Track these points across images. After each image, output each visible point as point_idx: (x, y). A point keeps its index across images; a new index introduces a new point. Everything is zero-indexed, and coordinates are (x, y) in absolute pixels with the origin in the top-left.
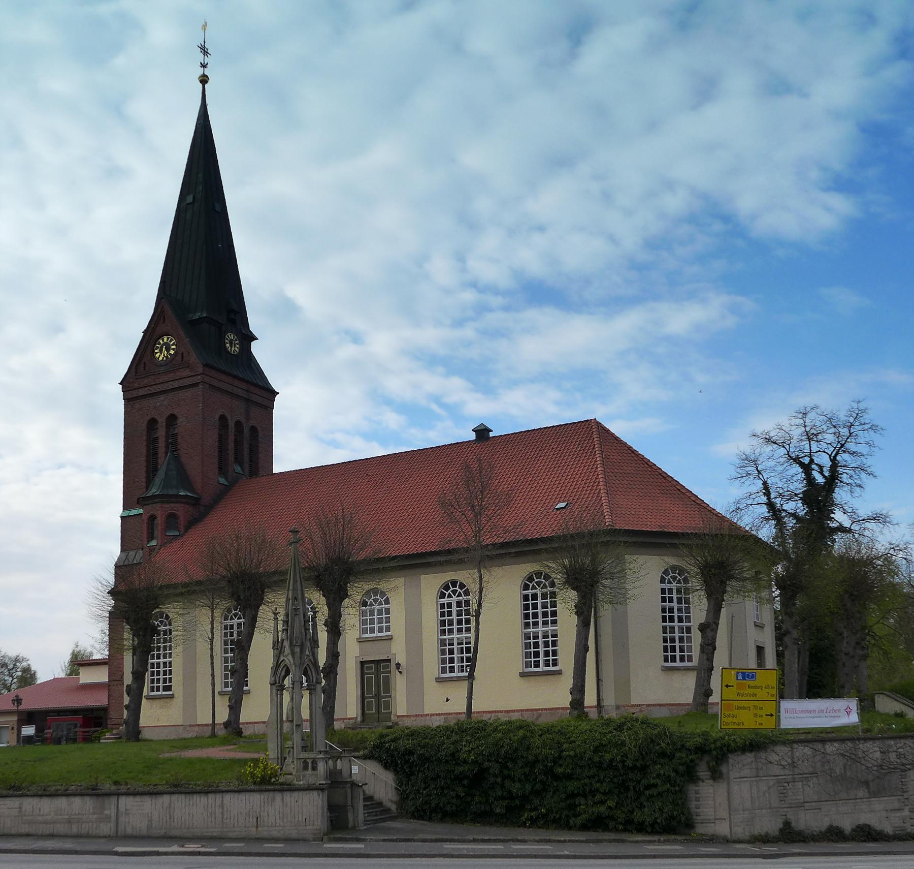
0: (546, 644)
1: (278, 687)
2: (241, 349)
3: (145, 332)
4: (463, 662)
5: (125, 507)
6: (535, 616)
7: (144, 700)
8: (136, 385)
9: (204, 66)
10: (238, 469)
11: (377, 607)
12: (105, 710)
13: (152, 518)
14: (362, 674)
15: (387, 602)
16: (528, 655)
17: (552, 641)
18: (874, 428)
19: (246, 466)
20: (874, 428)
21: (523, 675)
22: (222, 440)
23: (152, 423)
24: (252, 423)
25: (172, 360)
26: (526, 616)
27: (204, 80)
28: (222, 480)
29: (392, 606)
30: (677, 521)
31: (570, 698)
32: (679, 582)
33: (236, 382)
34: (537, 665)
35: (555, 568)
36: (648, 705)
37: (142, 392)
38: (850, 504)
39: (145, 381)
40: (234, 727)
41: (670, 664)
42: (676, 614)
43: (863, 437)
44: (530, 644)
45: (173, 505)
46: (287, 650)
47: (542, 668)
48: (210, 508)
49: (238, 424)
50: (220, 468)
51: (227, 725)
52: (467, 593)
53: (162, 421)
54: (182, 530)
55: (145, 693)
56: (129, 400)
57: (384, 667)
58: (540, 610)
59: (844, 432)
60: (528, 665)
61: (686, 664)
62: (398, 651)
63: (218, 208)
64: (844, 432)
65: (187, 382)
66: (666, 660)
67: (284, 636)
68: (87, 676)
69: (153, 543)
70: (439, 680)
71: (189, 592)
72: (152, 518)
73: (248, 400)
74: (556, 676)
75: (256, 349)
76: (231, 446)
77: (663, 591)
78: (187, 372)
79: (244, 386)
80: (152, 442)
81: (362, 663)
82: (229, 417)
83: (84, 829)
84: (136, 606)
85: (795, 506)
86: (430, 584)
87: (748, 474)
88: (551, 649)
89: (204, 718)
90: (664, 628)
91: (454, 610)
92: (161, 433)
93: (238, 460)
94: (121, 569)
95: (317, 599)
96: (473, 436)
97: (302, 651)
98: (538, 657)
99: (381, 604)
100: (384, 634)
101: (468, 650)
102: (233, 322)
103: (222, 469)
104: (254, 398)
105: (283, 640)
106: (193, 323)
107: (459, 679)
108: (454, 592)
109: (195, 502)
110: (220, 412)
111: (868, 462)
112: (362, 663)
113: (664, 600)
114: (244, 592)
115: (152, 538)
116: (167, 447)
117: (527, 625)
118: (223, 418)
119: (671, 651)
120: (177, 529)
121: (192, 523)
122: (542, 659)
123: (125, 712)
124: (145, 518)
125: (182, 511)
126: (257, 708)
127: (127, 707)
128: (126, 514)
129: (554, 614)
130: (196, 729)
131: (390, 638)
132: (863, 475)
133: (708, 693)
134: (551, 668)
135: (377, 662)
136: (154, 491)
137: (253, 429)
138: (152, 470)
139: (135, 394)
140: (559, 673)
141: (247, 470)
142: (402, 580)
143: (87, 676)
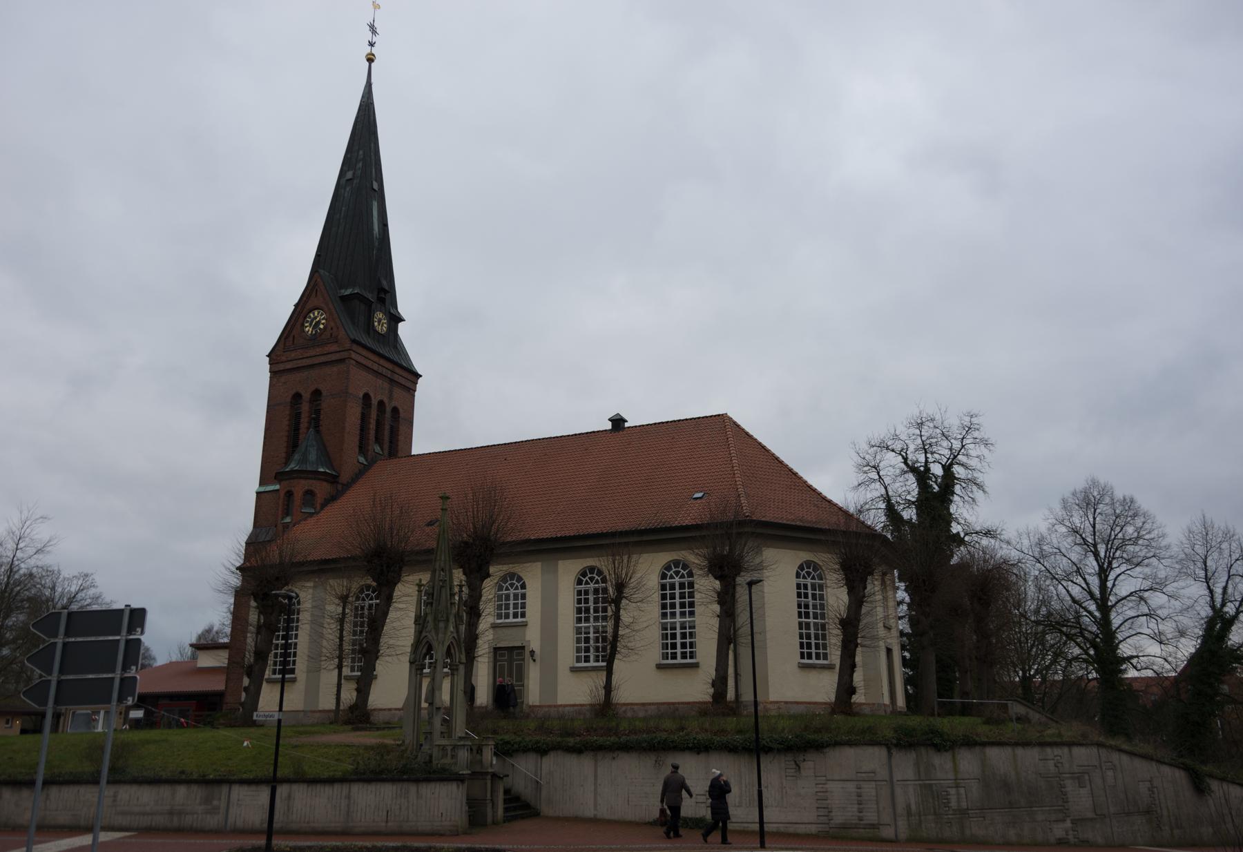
0: (684, 636)
1: (416, 665)
2: (389, 328)
3: (296, 306)
4: (604, 649)
5: (261, 483)
6: (673, 606)
7: (264, 684)
8: (284, 358)
9: (372, 44)
10: (378, 449)
11: (512, 591)
12: (220, 695)
13: (289, 494)
14: (495, 661)
15: (523, 587)
16: (665, 646)
17: (689, 633)
18: (986, 444)
19: (386, 446)
20: (986, 444)
21: (660, 667)
22: (364, 418)
23: (297, 397)
24: (394, 404)
25: (321, 334)
26: (664, 606)
27: (370, 59)
28: (362, 459)
29: (529, 592)
30: (808, 516)
31: (712, 691)
32: (813, 578)
33: (382, 362)
34: (674, 656)
35: (693, 558)
36: (786, 703)
37: (289, 366)
38: (968, 513)
39: (293, 355)
40: (359, 716)
41: (806, 661)
42: (811, 610)
43: (973, 450)
44: (668, 635)
45: (311, 481)
46: (430, 625)
47: (679, 660)
48: (347, 486)
49: (381, 403)
50: (360, 447)
51: (352, 708)
52: (604, 580)
53: (306, 396)
54: (318, 506)
55: (266, 677)
56: (274, 373)
57: (518, 654)
58: (677, 601)
59: (957, 445)
60: (665, 656)
61: (821, 662)
62: (533, 638)
63: (375, 186)
64: (957, 445)
65: (334, 357)
66: (802, 657)
67: (428, 610)
68: (207, 660)
69: (288, 520)
70: (574, 670)
71: (323, 568)
72: (289, 494)
73: (391, 381)
74: (688, 671)
75: (402, 329)
76: (373, 426)
77: (798, 586)
78: (334, 348)
79: (390, 366)
80: (296, 418)
81: (496, 649)
82: (372, 395)
83: (188, 821)
84: (265, 582)
85: (909, 514)
86: (568, 571)
87: (289, 797)
88: (688, 640)
89: (327, 702)
90: (800, 624)
91: (591, 597)
92: (305, 407)
93: (378, 440)
94: (253, 545)
95: (458, 576)
96: (609, 426)
97: (446, 628)
98: (677, 651)
99: (517, 588)
100: (519, 620)
101: (605, 639)
102: (382, 301)
103: (362, 449)
104: (396, 377)
105: (426, 614)
106: (344, 299)
107: (594, 669)
108: (592, 579)
109: (333, 479)
110: (364, 390)
111: (980, 478)
112: (496, 649)
113: (799, 595)
114: (382, 564)
115: (287, 515)
116: (310, 423)
117: (664, 615)
118: (367, 397)
119: (810, 648)
120: (313, 506)
121: (333, 498)
122: (679, 650)
123: (244, 694)
124: (282, 494)
125: (322, 489)
126: (391, 686)
127: (246, 689)
128: (263, 489)
129: (692, 605)
130: (317, 715)
131: (525, 625)
132: (975, 488)
133: (853, 691)
134: (688, 661)
135: (511, 649)
136: (293, 466)
137: (395, 410)
138: (293, 444)
139: (281, 367)
140: (696, 666)
141: (386, 452)
142: (539, 564)
143: (207, 660)
